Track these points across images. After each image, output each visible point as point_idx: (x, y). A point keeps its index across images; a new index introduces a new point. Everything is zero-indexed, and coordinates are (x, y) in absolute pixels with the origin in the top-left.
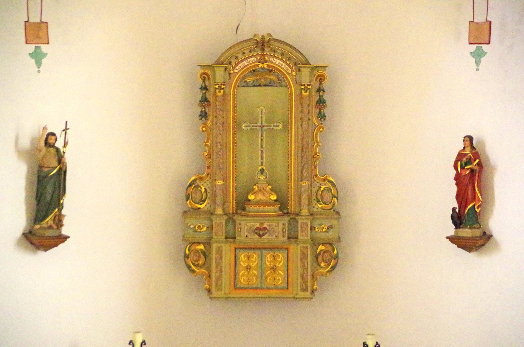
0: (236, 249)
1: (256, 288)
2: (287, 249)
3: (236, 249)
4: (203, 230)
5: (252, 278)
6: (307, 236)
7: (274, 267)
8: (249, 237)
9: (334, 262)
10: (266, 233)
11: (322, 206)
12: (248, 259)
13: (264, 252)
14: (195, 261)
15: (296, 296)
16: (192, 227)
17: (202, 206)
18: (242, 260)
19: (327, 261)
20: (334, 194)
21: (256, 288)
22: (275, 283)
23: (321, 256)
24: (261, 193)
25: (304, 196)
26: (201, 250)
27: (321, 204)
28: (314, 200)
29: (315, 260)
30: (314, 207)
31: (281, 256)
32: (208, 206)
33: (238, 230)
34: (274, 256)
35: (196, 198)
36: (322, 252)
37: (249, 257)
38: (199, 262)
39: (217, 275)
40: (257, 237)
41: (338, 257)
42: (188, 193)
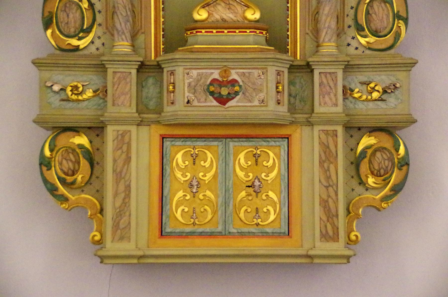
0: (163, 138)
1: (211, 235)
2: (288, 138)
3: (163, 138)
4: (85, 96)
5: (202, 210)
6: (336, 105)
7: (257, 183)
8: (195, 103)
9: (396, 176)
10: (237, 93)
11: (367, 39)
12: (194, 164)
13: (231, 144)
14: (66, 174)
15: (311, 253)
16: (56, 88)
17: (82, 43)
18: (177, 164)
19: (382, 172)
20: (398, 12)
21: (211, 235)
22: (260, 220)
23: (366, 160)
24: (223, 4)
25: (327, 9)
26: (81, 146)
27: (365, 37)
28: (349, 27)
29: (353, 173)
30: (349, 45)
31: (271, 154)
32: (98, 43)
33: (168, 89)
34: (254, 155)
35: (67, 23)
36: (370, 152)
37: (194, 158)
38: (75, 177)
39: (118, 203)
40: (215, 103)
41: (408, 164)
42: (47, 10)
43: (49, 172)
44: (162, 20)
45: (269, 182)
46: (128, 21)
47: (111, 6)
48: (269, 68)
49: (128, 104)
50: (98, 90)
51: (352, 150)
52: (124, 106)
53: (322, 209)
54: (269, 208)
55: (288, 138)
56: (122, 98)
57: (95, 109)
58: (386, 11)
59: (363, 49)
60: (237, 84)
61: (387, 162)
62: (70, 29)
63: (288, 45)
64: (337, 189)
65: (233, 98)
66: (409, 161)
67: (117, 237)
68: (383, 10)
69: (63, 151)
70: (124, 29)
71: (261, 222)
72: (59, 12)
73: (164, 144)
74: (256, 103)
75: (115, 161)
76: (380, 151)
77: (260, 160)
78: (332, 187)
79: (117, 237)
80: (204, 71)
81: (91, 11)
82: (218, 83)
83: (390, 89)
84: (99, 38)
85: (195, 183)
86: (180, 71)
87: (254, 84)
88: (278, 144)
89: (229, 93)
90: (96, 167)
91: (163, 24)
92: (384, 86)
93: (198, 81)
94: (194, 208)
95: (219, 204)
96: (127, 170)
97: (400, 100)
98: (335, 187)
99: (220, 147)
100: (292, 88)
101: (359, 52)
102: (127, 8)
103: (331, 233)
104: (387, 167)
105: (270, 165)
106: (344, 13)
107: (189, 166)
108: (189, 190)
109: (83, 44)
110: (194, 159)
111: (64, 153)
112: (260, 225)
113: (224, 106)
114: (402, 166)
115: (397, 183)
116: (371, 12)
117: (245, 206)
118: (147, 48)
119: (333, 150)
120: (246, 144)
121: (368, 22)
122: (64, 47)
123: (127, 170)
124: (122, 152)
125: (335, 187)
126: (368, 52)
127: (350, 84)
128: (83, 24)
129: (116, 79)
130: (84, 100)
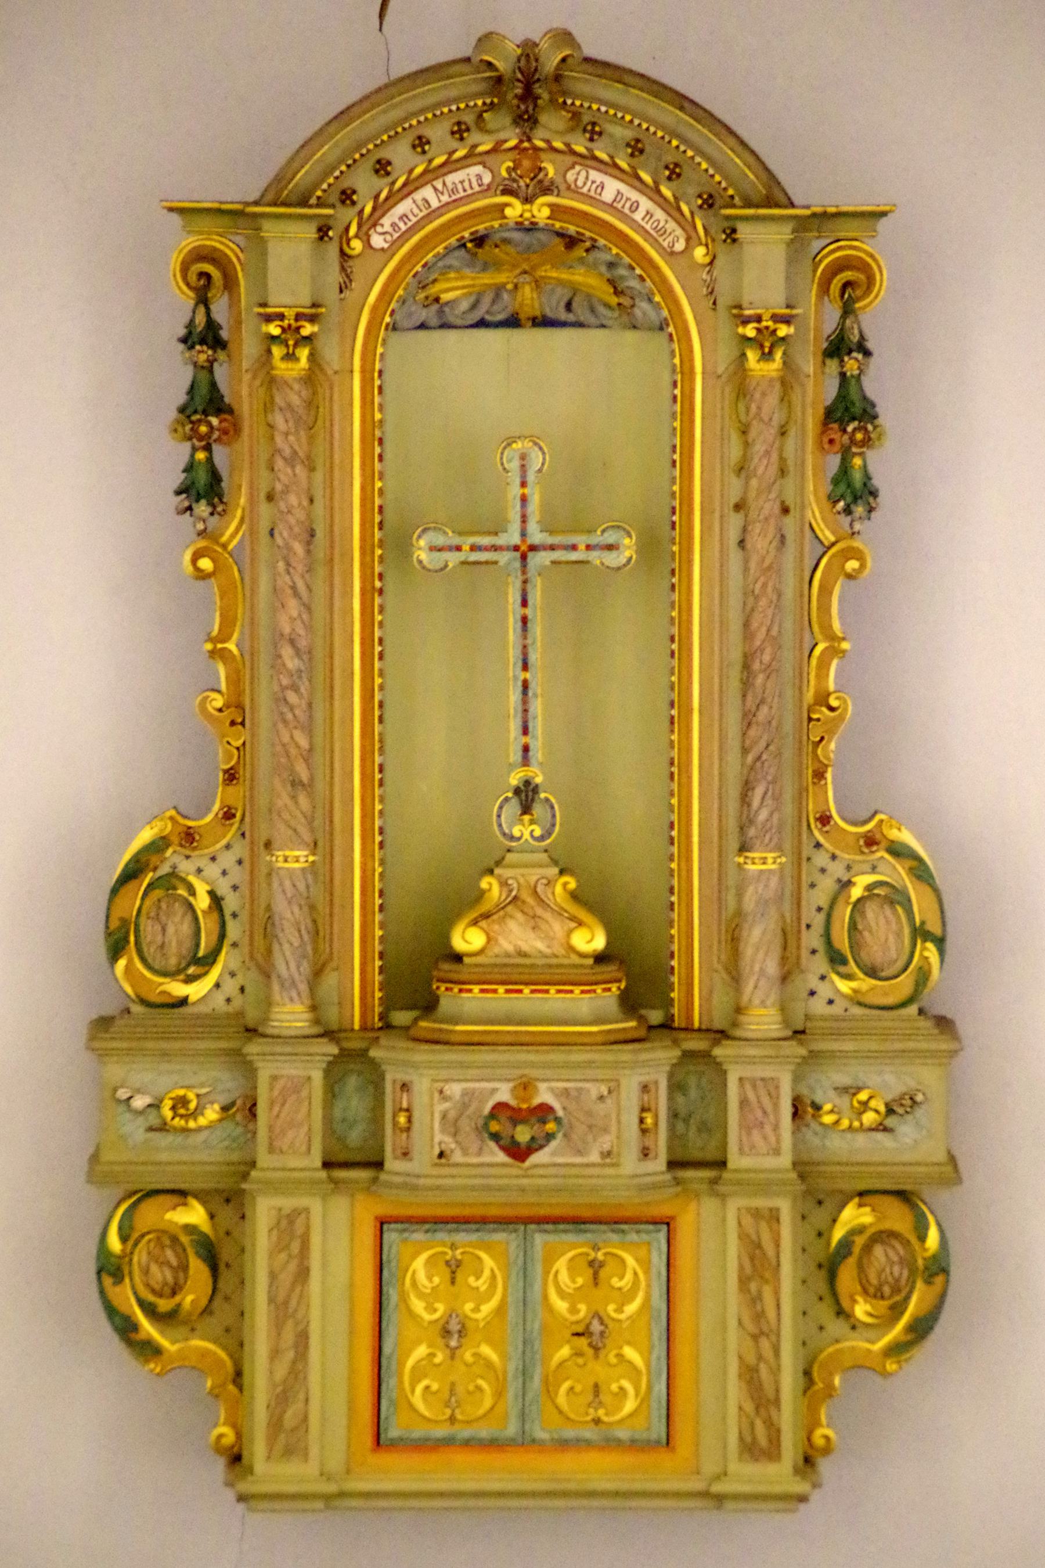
1: (493, 1444)
2: (668, 1223)
3: (382, 1224)
4: (202, 1121)
5: (471, 1388)
6: (777, 1152)
7: (596, 1327)
8: (458, 1157)
9: (920, 1300)
10: (550, 1137)
11: (854, 984)
12: (453, 1282)
13: (539, 1239)
15: (717, 1488)
16: (140, 1102)
17: (194, 991)
18: (414, 1283)
20: (923, 923)
21: (493, 1444)
22: (601, 1412)
23: (851, 1261)
26: (190, 1229)
27: (849, 977)
28: (814, 952)
29: (822, 1287)
30: (812, 993)
31: (630, 1261)
32: (230, 987)
33: (395, 1123)
34: (591, 1263)
35: (162, 946)
36: (860, 1241)
37: (454, 1268)
38: (177, 1299)
39: (281, 1371)
40: (501, 1157)
41: (945, 1271)
43: (118, 1289)
44: (379, 933)
45: (625, 1325)
46: (304, 956)
47: (263, 906)
48: (624, 1082)
49: (304, 1148)
50: (233, 1104)
51: (820, 1234)
52: (294, 1153)
53: (744, 1385)
54: (626, 1384)
55: (668, 1223)
56: (290, 1134)
57: (227, 1148)
58: (894, 926)
59: (845, 1003)
60: (551, 1117)
61: (896, 1269)
62: (167, 959)
63: (673, 990)
64: (778, 1341)
65: (541, 1147)
66: (948, 1265)
67: (279, 1446)
68: (888, 922)
69: (150, 1241)
70: (296, 976)
71: (607, 1414)
72: (143, 919)
73: (385, 1236)
74: (594, 1157)
75: (273, 1276)
76: (883, 1242)
77: (603, 1273)
78: (768, 1336)
79: (279, 1446)
80: (477, 1085)
81: (215, 915)
82: (509, 1113)
83: (902, 1105)
84: (233, 975)
85: (454, 1326)
86: (422, 1085)
87: (589, 1114)
88: (645, 1237)
89: (533, 1138)
90: (226, 1276)
91: (381, 943)
92: (889, 1097)
93: (465, 1106)
94: (453, 1384)
95: (510, 1375)
96: (301, 1296)
97: (924, 1132)
98: (773, 1338)
99: (513, 1246)
100: (680, 1099)
101: (837, 1009)
102: (303, 928)
103: (763, 1441)
104: (897, 1280)
105: (627, 1284)
106: (799, 919)
107: (442, 1287)
108: (440, 1342)
109: (196, 993)
110: (453, 1272)
111: (152, 1245)
112: (603, 1422)
113: (520, 1164)
114: (932, 1276)
115: (922, 1314)
116: (860, 927)
117: (567, 1378)
118: (344, 1001)
119: (770, 1252)
120: (570, 1238)
121: (855, 945)
122: (153, 998)
123: (301, 1296)
124: (290, 1256)
125: (773, 1338)
126: (857, 1011)
127: (812, 1089)
128: (197, 945)
129: (276, 1093)
130: (200, 1129)
